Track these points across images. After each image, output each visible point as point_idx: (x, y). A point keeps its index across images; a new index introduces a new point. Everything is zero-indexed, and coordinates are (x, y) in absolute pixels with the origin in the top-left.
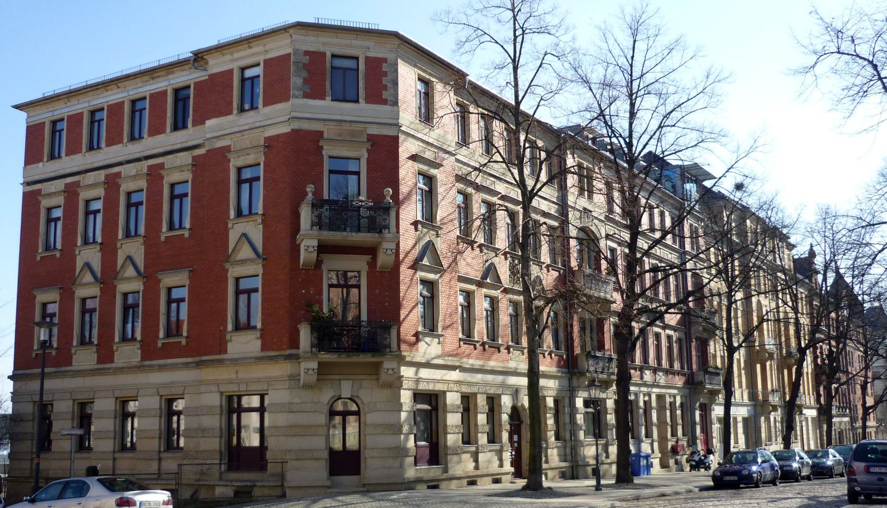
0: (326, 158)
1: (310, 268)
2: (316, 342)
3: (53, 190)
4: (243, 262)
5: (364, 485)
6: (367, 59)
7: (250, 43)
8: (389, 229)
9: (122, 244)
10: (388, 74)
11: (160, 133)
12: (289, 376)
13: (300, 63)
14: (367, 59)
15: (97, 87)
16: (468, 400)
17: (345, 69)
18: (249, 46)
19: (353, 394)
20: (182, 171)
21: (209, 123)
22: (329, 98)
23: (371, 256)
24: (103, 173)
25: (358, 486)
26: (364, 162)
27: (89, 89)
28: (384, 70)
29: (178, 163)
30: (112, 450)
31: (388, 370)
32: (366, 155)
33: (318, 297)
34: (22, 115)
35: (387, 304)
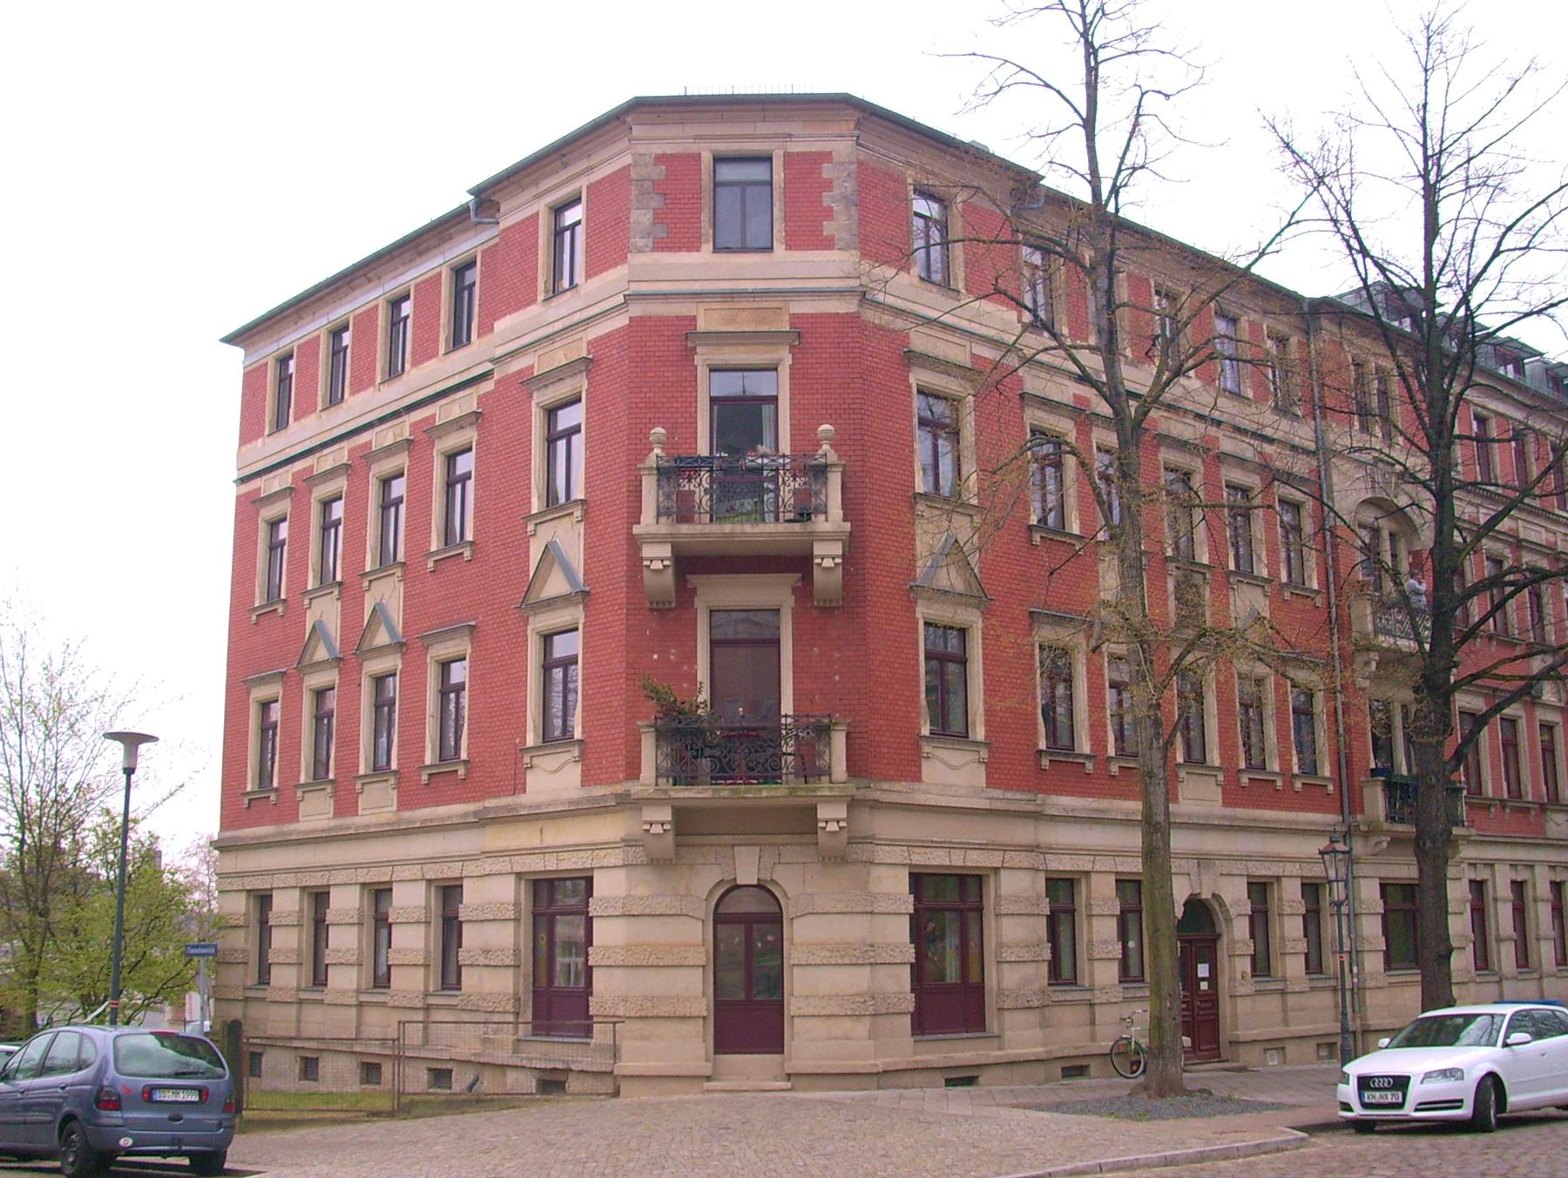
0: (702, 372)
1: (667, 606)
2: (667, 764)
3: (276, 487)
4: (551, 603)
5: (789, 1076)
6: (788, 156)
7: (563, 156)
8: (826, 513)
9: (370, 581)
10: (835, 184)
11: (430, 358)
12: (623, 840)
13: (648, 180)
14: (788, 156)
15: (337, 285)
16: (1260, 889)
17: (744, 185)
18: (562, 163)
19: (762, 877)
20: (462, 428)
21: (499, 325)
22: (708, 247)
23: (800, 575)
24: (346, 445)
25: (776, 1079)
26: (784, 371)
27: (325, 291)
28: (824, 176)
29: (456, 412)
30: (355, 987)
31: (827, 822)
32: (788, 360)
33: (685, 668)
34: (237, 353)
35: (837, 678)
